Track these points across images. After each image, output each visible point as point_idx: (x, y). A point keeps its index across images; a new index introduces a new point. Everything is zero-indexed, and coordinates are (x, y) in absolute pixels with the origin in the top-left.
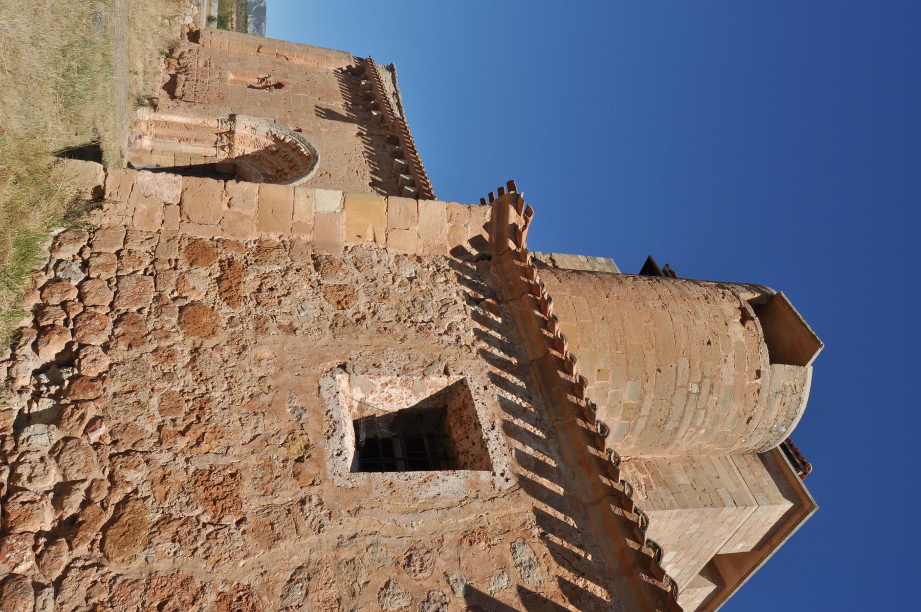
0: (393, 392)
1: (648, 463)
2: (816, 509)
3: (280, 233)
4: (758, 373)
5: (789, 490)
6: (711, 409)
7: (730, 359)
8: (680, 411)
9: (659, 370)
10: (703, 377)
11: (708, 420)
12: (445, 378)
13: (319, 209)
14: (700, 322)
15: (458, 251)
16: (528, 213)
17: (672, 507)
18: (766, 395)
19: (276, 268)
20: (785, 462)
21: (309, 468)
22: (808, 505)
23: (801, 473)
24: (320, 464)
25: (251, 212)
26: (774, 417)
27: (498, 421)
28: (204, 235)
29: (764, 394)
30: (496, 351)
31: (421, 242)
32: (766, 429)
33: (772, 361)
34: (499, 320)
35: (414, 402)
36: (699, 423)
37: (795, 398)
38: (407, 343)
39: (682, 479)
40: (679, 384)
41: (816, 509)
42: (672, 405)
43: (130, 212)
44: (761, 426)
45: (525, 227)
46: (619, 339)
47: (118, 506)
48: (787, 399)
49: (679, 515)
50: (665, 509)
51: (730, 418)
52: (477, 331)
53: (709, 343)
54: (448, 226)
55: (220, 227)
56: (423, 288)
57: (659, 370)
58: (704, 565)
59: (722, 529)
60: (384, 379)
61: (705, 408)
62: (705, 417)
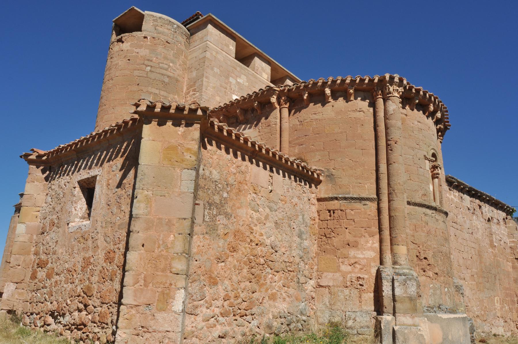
0: (79, 207)
1: (188, 89)
2: (211, 14)
3: (32, 247)
4: (145, 37)
5: (203, 26)
6: (159, 61)
7: (137, 51)
8: (159, 75)
9: (138, 84)
10: (144, 64)
11: (165, 62)
12: (76, 189)
13: (24, 232)
14: (120, 64)
15: (46, 179)
16: (33, 150)
17: (202, 81)
18: (156, 34)
19: (42, 248)
20: (193, 24)
21: (86, 237)
22: (209, 18)
23: (200, 17)
24: (85, 232)
25: (22, 258)
26: (168, 31)
27: (88, 171)
28: (29, 275)
29: (155, 35)
30: (73, 169)
31: (41, 194)
32: (174, 34)
33: (141, 31)
34: (66, 166)
35: (84, 200)
36: (167, 66)
37: (159, 21)
38: (66, 201)
39: (194, 74)
40: (145, 76)
41: (211, 14)
42: (155, 79)
43: (18, 301)
44: (172, 37)
45: (38, 152)
46: (122, 102)
47: (84, 294)
48: (159, 24)
49: (207, 77)
50: (202, 84)
51: (166, 52)
52: (67, 176)
53: (129, 60)
54: (36, 183)
55: (28, 269)
56: (54, 194)
57: (138, 84)
58: (241, 64)
59: (219, 56)
60: (73, 210)
61: (159, 63)
62: (163, 63)
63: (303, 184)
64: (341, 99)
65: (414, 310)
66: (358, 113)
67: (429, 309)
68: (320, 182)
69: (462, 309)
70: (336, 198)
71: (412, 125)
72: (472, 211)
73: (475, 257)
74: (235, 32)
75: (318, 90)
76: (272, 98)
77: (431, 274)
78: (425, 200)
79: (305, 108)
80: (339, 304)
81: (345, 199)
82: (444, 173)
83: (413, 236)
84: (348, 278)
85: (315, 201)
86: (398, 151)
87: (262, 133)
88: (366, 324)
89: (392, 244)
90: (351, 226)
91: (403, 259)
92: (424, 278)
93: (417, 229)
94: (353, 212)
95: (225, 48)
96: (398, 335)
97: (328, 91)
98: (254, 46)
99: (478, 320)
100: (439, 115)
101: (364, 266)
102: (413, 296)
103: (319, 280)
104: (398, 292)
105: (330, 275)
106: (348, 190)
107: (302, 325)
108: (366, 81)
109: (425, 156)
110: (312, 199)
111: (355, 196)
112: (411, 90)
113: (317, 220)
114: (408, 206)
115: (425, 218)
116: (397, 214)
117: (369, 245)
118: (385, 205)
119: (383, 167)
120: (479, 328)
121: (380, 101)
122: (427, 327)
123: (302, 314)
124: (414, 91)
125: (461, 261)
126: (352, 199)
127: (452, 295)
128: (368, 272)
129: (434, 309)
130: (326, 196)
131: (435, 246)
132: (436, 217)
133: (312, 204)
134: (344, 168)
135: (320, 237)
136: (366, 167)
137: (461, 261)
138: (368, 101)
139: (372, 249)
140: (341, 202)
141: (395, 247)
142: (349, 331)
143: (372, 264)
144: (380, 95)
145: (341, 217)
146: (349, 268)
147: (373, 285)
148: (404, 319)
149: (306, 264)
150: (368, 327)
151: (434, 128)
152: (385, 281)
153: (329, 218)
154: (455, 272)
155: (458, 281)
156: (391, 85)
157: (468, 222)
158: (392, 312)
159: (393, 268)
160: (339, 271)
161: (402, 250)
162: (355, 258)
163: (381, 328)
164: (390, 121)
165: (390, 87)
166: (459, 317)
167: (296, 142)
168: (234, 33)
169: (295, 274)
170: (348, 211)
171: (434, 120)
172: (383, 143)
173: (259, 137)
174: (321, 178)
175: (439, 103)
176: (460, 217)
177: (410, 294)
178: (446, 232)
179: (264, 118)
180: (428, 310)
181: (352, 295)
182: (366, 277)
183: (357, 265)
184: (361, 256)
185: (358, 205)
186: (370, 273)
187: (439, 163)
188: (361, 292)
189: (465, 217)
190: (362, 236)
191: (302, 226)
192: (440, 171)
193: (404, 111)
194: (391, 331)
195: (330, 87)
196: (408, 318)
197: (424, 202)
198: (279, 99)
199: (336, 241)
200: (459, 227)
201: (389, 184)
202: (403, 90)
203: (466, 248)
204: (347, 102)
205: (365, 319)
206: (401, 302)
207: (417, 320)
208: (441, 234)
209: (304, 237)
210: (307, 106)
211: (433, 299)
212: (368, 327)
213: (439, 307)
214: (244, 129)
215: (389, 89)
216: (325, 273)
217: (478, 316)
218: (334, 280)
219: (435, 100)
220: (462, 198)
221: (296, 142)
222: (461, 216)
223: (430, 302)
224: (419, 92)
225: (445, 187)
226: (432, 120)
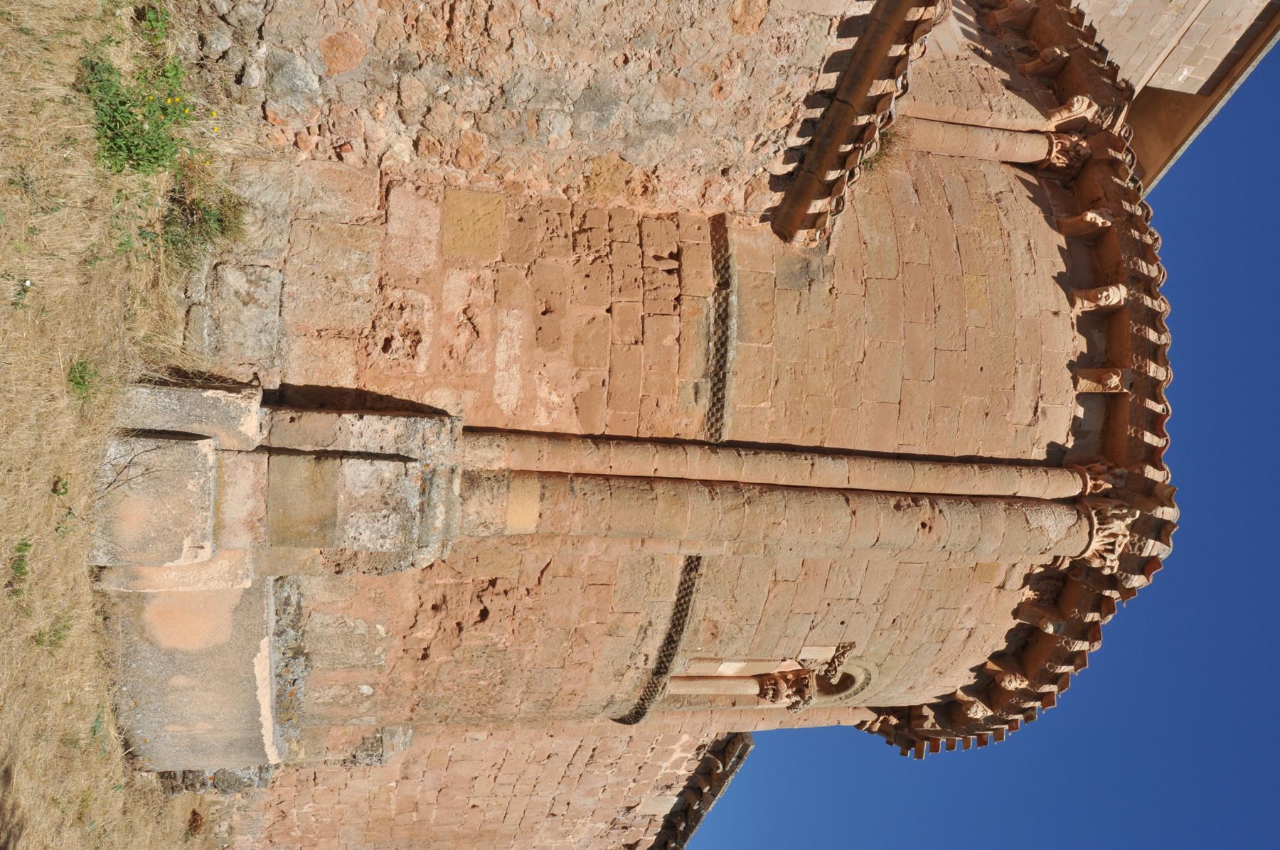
63: (795, 141)
64: (1081, 345)
65: (279, 532)
66: (1029, 402)
67: (291, 610)
68: (785, 235)
69: (302, 755)
70: (724, 284)
71: (965, 607)
72: (623, 820)
73: (474, 819)
74: (1236, 87)
75: (1119, 264)
76: (1087, 101)
77: (426, 632)
78: (696, 632)
79: (1047, 219)
80: (315, 250)
81: (723, 318)
82: (762, 727)
83: (570, 574)
84: (415, 296)
85: (712, 210)
86: (901, 529)
87: (954, 64)
88: (230, 344)
89: (544, 475)
90: (616, 329)
91: (488, 512)
92: (411, 603)
93: (593, 590)
94: (669, 340)
95: (1187, 48)
96: (177, 450)
97: (1116, 295)
98: (1172, 163)
99: (270, 816)
100: (979, 711)
101: (463, 363)
102: (338, 533)
103: (409, 187)
104: (356, 471)
105: (430, 229)
106: (754, 333)
107: (224, 55)
108: (1149, 438)
109: (852, 645)
110: (727, 188)
111: (731, 355)
112: (1096, 608)
113: (642, 207)
114: (681, 563)
115: (631, 624)
116: (661, 504)
117: (543, 392)
118: (696, 465)
119: (833, 473)
120: (244, 817)
121: (1070, 485)
122: (213, 585)
123: (275, 68)
124: (1092, 617)
125: (464, 770)
126: (722, 344)
127: (346, 713)
128: (437, 377)
129: (292, 633)
130: (733, 250)
131: (527, 658)
132: (632, 673)
133: (708, 184)
134: (836, 328)
135: (579, 213)
136: (834, 411)
137: (464, 770)
138: (1070, 445)
139: (529, 401)
140: (711, 300)
141: (535, 485)
142: (203, 274)
143: (469, 396)
144: (1096, 487)
145: (654, 294)
146: (455, 305)
147: (385, 391)
148: (245, 486)
149: (477, 125)
150: (217, 349)
151: (924, 694)
152: (400, 430)
153: (650, 252)
154: (430, 744)
155: (398, 748)
156: (1132, 528)
157: (590, 802)
158: (275, 444)
159: (453, 471)
160: (447, 264)
161: (522, 512)
162: (496, 332)
163: (205, 387)
164: (1003, 514)
165: (1129, 521)
166: (261, 726)
167: (927, 177)
168: (1232, 84)
169: (440, 48)
170: (675, 324)
171: (960, 694)
172: (928, 483)
173: (938, 56)
174: (802, 235)
175: (1023, 711)
176: (610, 777)
177: (345, 522)
178: (573, 707)
179: (1007, 77)
180: (287, 602)
181: (350, 305)
182: (421, 366)
183: (466, 334)
184: (501, 357)
185: (696, 364)
186: (435, 385)
187: (812, 702)
188: (361, 340)
189: (607, 795)
190: (580, 368)
191: (631, 116)
192: (784, 702)
193: (1017, 579)
194: (195, 428)
195: (1132, 305)
196: (250, 504)
197: (692, 625)
198: (1080, 127)
199: (562, 263)
200: (575, 772)
201: (772, 487)
202: (1107, 572)
203: (508, 791)
204: (1071, 366)
205: (250, 342)
206: (314, 483)
207: (243, 540)
208: (569, 687)
209: (585, 124)
210: (1058, 227)
211: (330, 631)
212: (217, 349)
213: (298, 652)
214: (960, 18)
215: (1122, 518)
216: (438, 211)
217: (283, 815)
218: (411, 242)
219: (1040, 697)
220: (669, 787)
221: (927, 177)
222: (612, 780)
223: (318, 618)
224: (1084, 638)
225: (716, 729)
226: (964, 689)
